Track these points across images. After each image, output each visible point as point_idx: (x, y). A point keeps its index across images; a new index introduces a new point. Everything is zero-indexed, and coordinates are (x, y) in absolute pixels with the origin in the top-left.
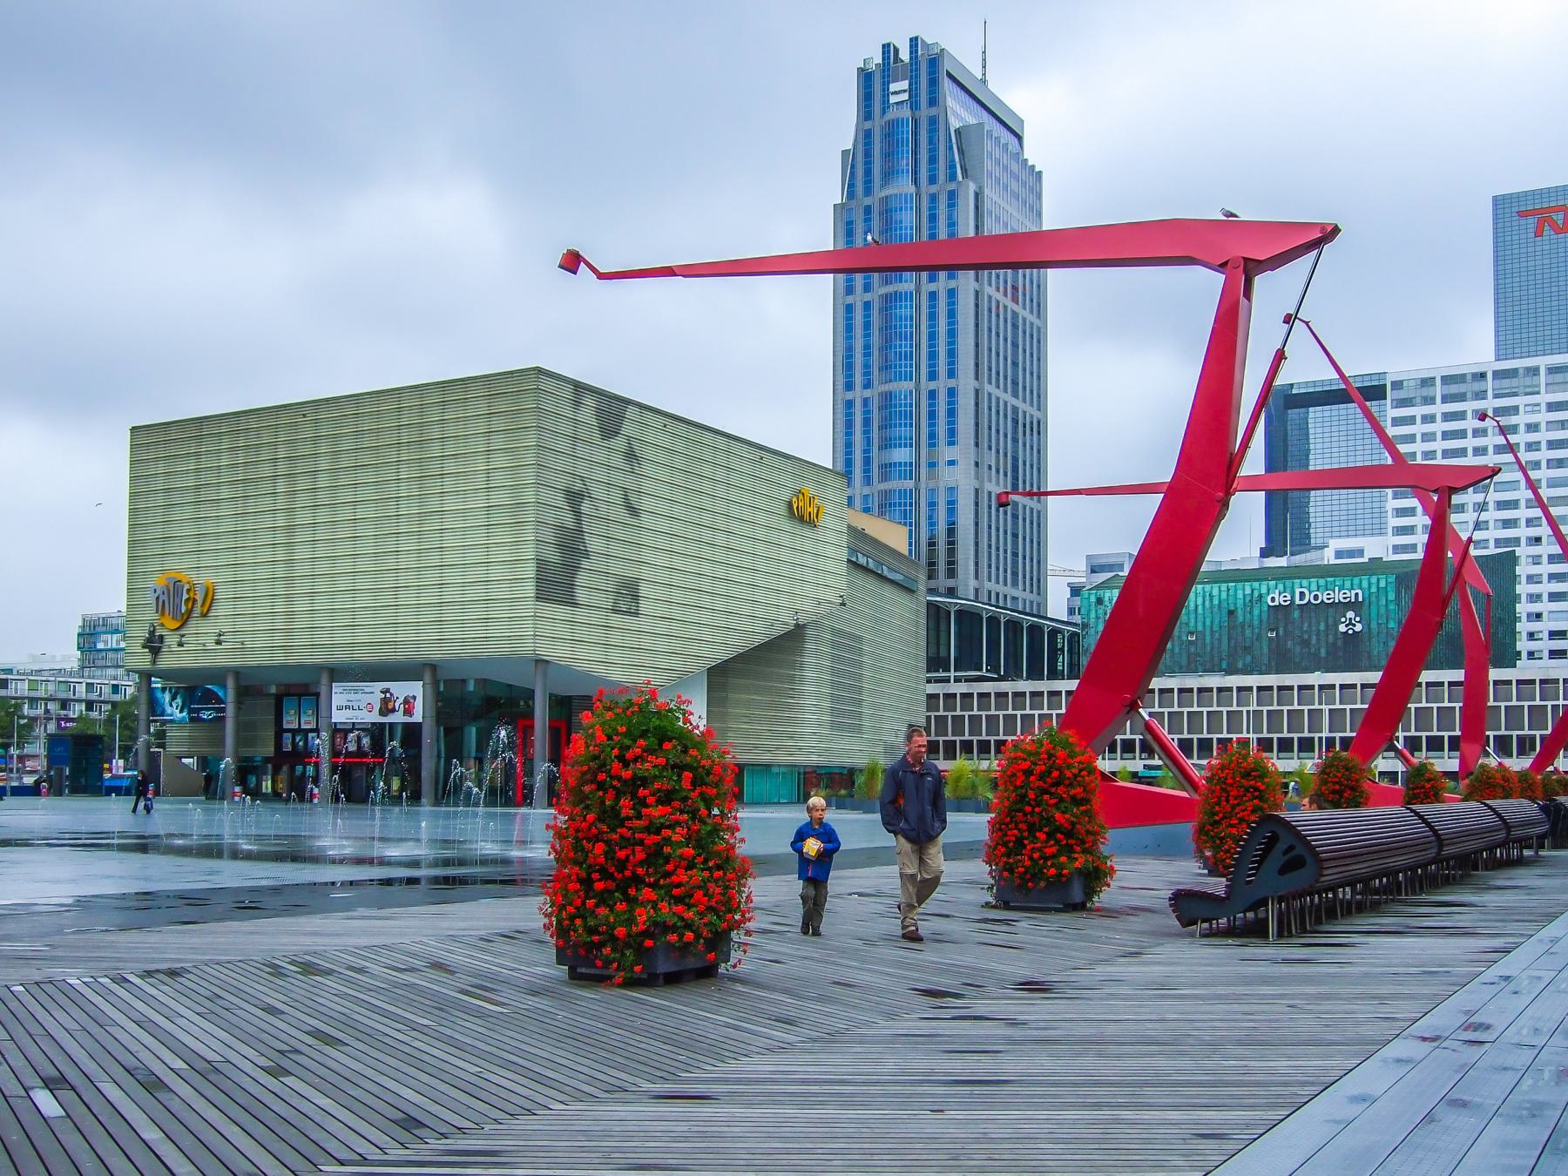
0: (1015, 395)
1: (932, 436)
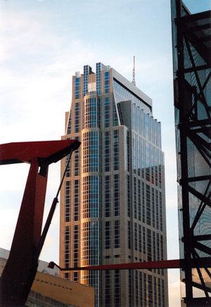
0: (149, 223)
1: (108, 243)
